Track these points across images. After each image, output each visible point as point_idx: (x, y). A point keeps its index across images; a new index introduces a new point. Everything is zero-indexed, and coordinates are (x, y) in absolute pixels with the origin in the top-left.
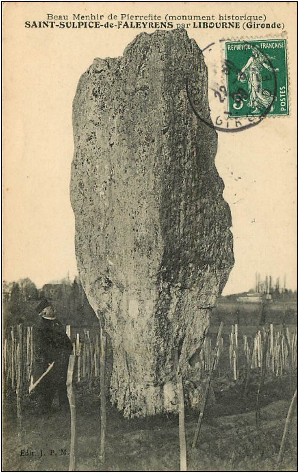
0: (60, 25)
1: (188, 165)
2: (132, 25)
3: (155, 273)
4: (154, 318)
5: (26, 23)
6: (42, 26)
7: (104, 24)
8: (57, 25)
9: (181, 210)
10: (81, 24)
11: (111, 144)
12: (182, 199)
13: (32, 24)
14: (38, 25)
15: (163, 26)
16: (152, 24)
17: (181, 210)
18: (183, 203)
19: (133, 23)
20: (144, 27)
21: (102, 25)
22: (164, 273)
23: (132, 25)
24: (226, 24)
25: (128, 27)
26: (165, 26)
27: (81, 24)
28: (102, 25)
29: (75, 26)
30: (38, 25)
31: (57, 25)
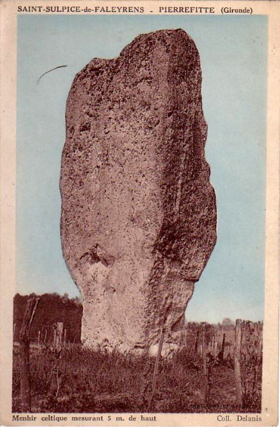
0: (46, 9)
1: (186, 148)
2: (107, 10)
3: (153, 243)
4: (147, 285)
5: (19, 8)
6: (31, 10)
7: (83, 9)
8: (44, 10)
9: (178, 188)
10: (162, 8)
11: (115, 292)
12: (115, 62)
13: (23, 8)
14: (28, 10)
15: (136, 10)
16: (126, 8)
17: (178, 188)
18: (180, 182)
19: (39, 10)
20: (119, 11)
21: (82, 10)
22: (160, 245)
23: (107, 10)
24: (183, 8)
25: (104, 11)
26: (138, 11)
27: (162, 8)
28: (82, 10)
29: (59, 10)
30: (28, 10)
31: (44, 10)
